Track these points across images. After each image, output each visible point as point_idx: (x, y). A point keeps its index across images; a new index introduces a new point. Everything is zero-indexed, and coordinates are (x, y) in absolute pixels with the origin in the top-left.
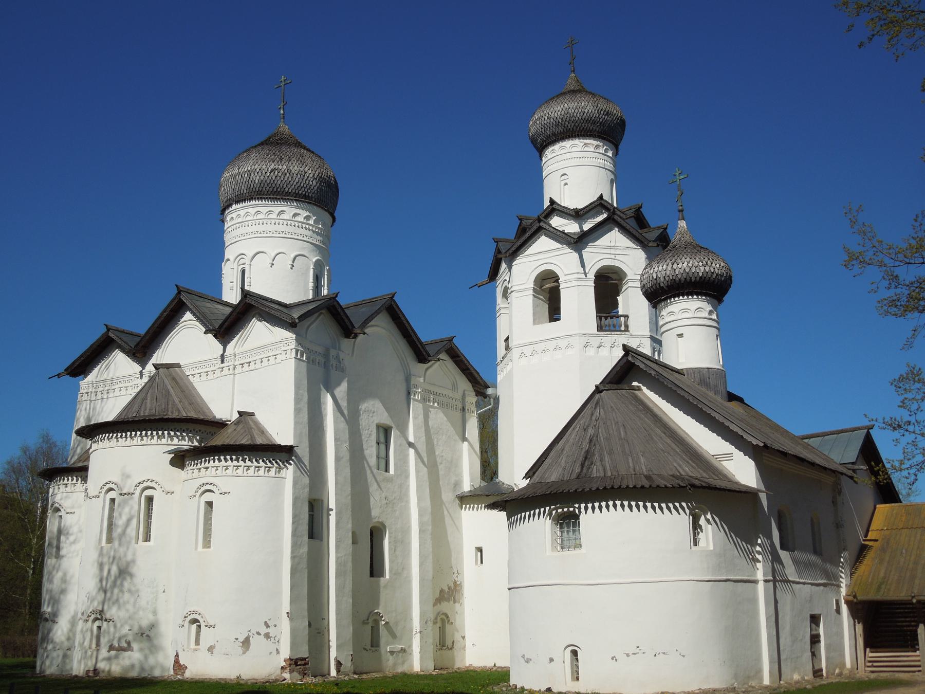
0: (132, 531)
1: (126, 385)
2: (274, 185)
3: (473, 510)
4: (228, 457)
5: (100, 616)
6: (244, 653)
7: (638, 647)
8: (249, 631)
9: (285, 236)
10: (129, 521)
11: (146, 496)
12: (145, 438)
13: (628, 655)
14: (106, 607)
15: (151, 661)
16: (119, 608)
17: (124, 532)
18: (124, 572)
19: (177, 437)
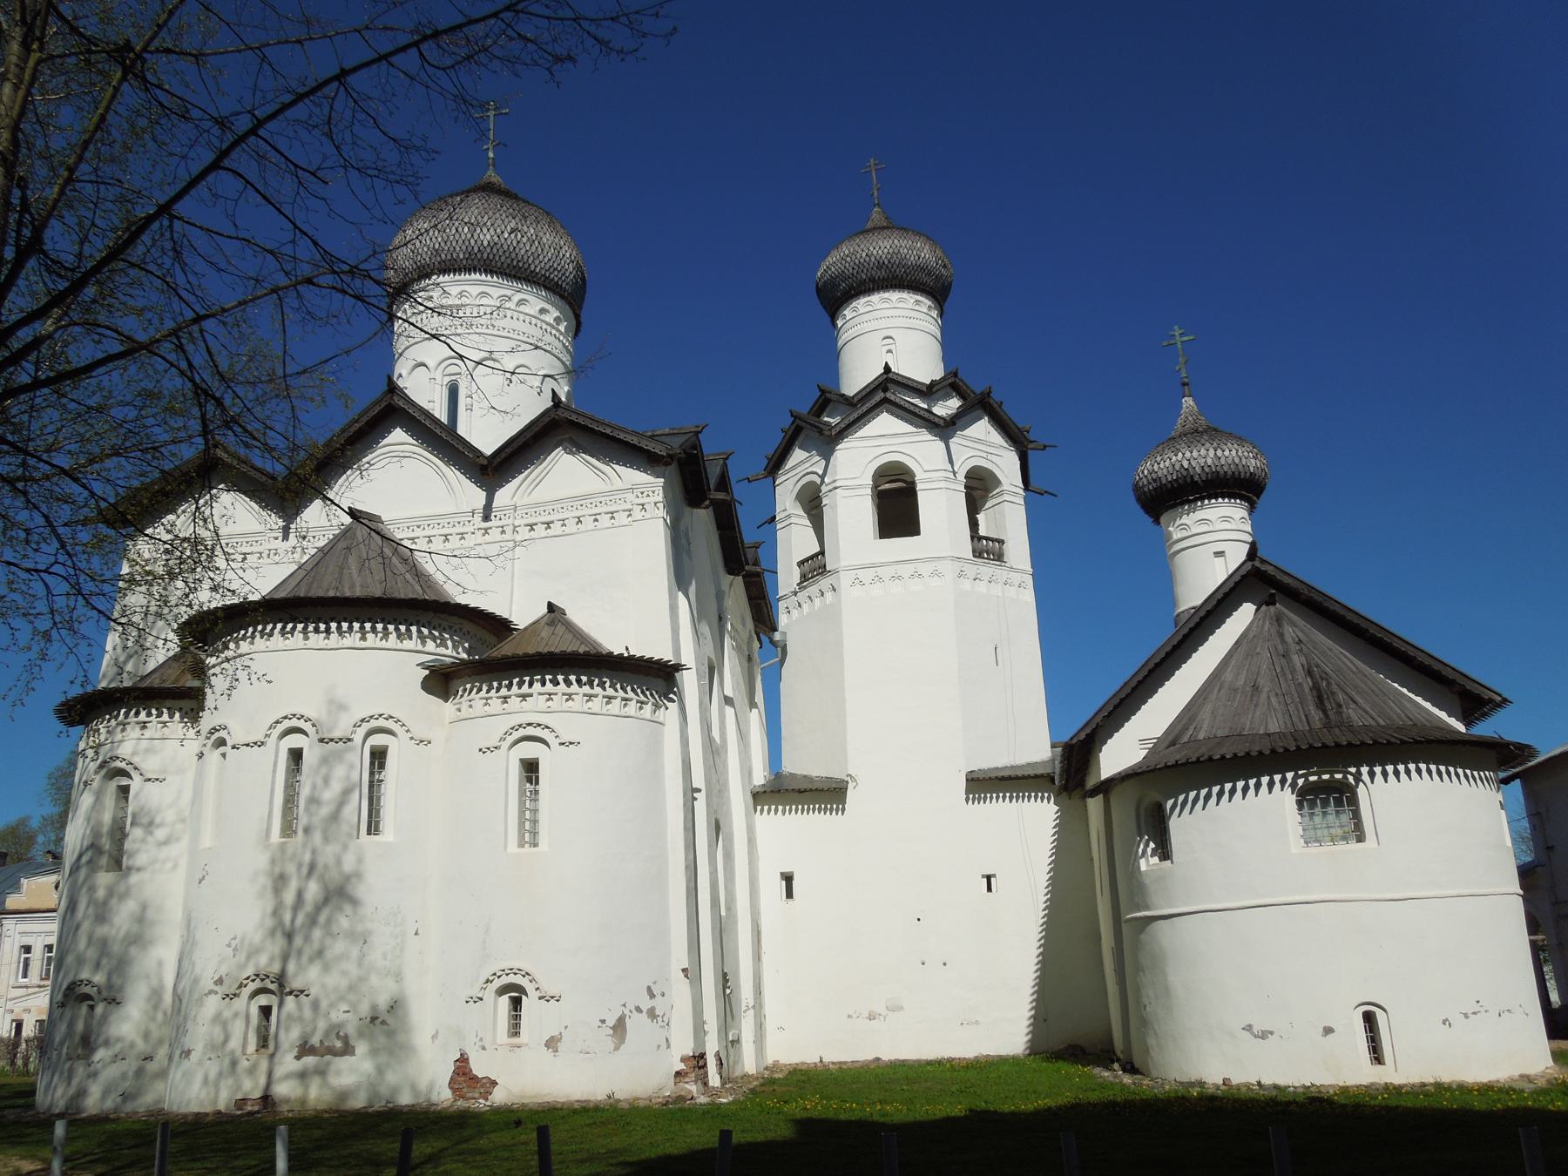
0: (349, 812)
2: (513, 255)
3: (769, 813)
4: (573, 678)
5: (279, 985)
6: (617, 1048)
7: (1478, 1002)
8: (624, 1005)
9: (527, 340)
10: (346, 792)
11: (372, 747)
12: (370, 636)
13: (1466, 1016)
14: (291, 967)
15: (391, 1078)
16: (326, 968)
17: (335, 816)
18: (339, 894)
19: (434, 639)
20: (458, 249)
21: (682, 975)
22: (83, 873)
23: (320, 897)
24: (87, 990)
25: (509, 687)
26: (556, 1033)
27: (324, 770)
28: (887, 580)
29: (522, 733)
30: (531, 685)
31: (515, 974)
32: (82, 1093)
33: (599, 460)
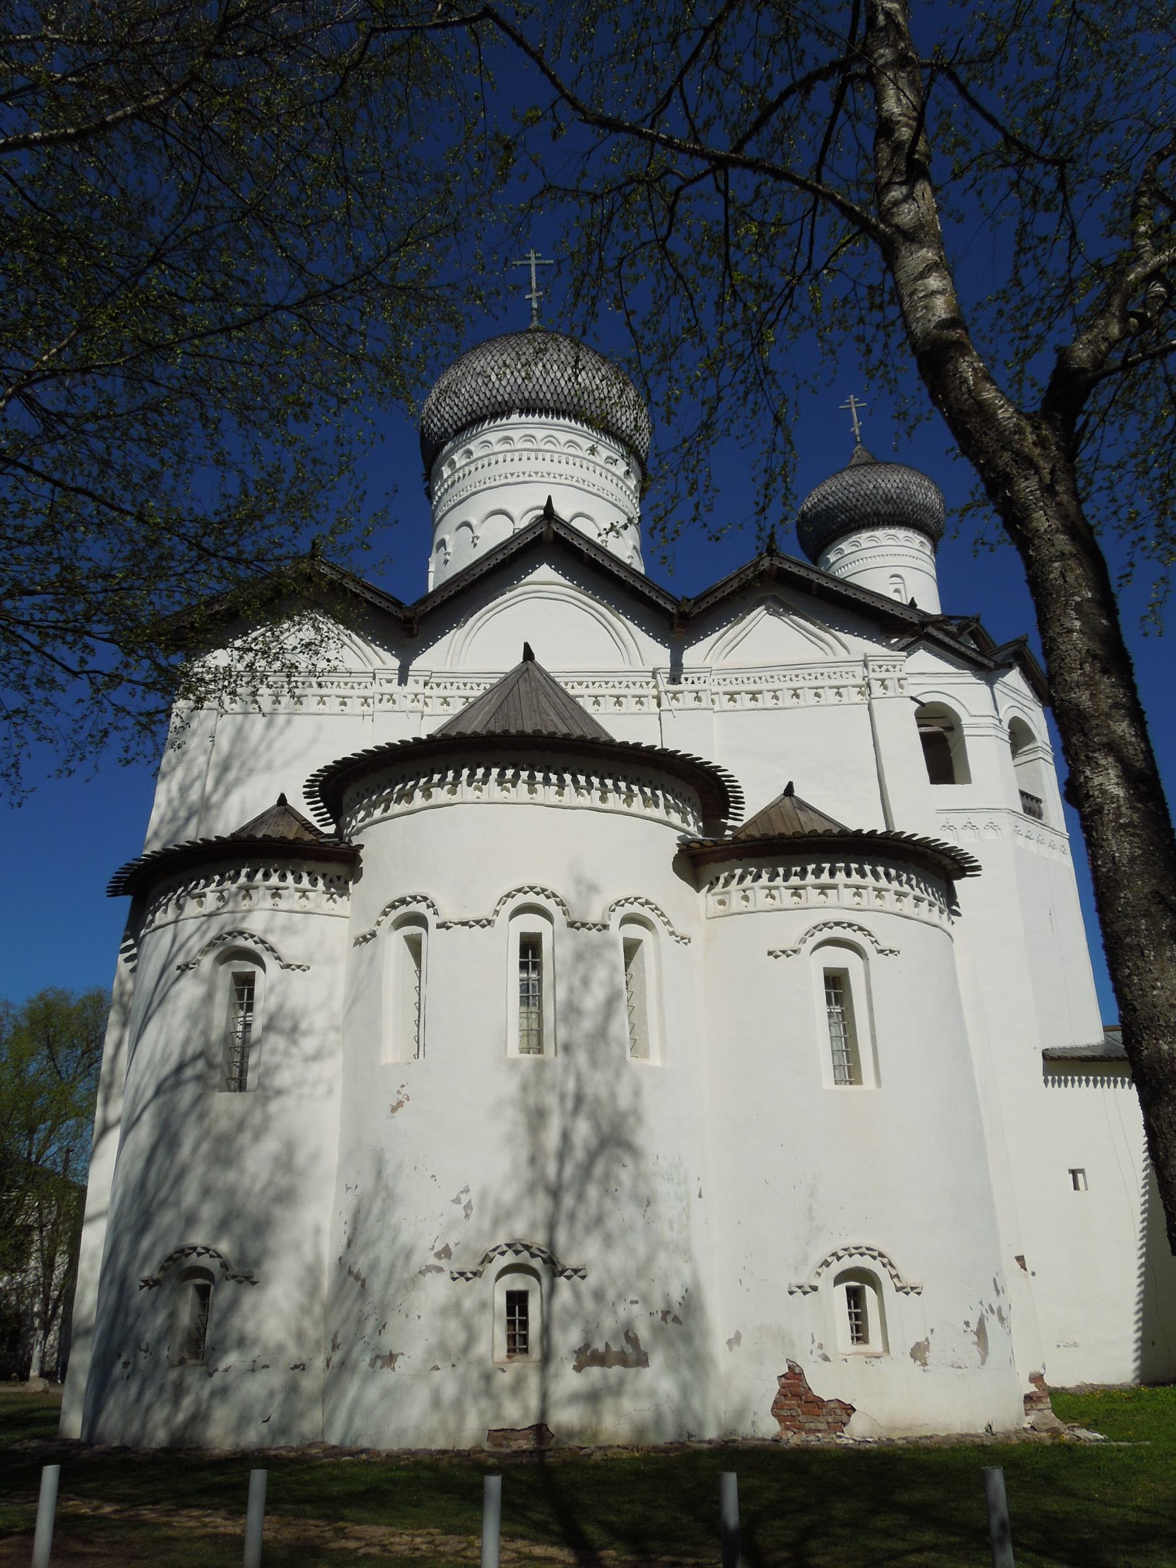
1: (345, 691)
14: (562, 1237)
16: (608, 1241)
20: (545, 388)
21: (1017, 1265)
22: (188, 1093)
23: (593, 1142)
24: (205, 1261)
25: (803, 874)
26: (921, 1339)
27: (581, 969)
28: (959, 828)
29: (827, 934)
30: (832, 874)
31: (862, 1254)
32: (200, 1417)
33: (814, 624)
